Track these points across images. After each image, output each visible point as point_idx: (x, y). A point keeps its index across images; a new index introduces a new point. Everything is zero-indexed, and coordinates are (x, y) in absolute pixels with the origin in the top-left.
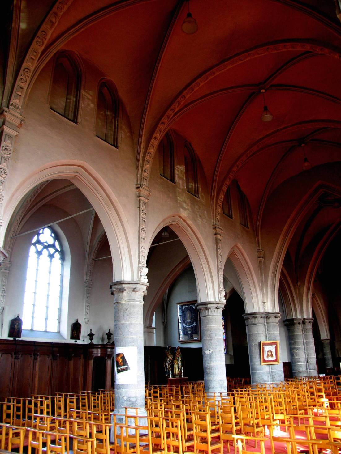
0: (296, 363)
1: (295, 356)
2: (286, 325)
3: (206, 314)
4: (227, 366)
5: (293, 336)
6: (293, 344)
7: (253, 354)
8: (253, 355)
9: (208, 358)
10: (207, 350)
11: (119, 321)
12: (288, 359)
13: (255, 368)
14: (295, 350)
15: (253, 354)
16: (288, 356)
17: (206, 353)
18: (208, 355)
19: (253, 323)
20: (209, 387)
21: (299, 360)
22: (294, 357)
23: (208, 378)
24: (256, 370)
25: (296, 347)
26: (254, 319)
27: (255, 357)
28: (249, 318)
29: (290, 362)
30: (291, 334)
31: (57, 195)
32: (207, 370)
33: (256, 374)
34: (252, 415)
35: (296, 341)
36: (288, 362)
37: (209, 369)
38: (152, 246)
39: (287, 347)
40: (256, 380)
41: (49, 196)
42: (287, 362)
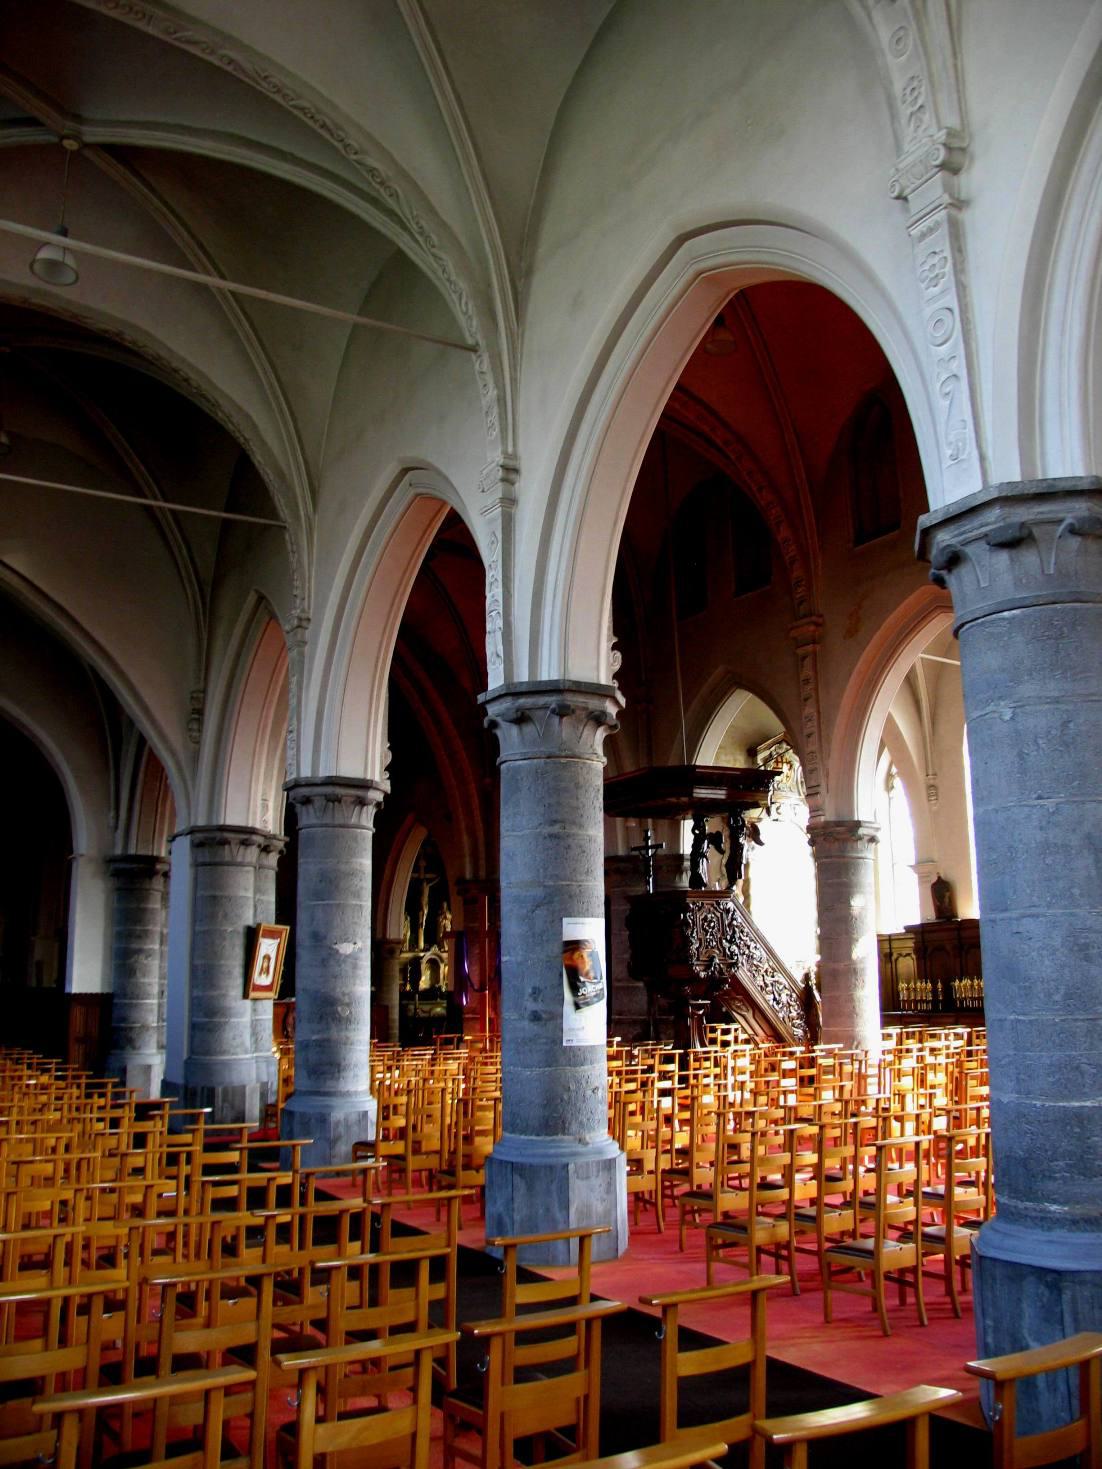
0: (138, 998)
1: (138, 974)
2: (116, 874)
3: (354, 820)
4: (372, 992)
5: (145, 910)
6: (139, 937)
7: (222, 962)
8: (221, 966)
9: (347, 967)
10: (346, 940)
11: (581, 826)
12: (103, 985)
13: (230, 1008)
14: (142, 957)
15: (222, 962)
16: (104, 974)
17: (341, 951)
18: (347, 956)
19: (239, 859)
20: (343, 1064)
21: (148, 988)
22: (133, 980)
23: (343, 1034)
24: (224, 1015)
25: (146, 947)
26: (242, 848)
27: (230, 973)
28: (229, 843)
29: (108, 994)
30: (133, 906)
31: (364, 216)
32: (339, 1009)
33: (227, 1027)
34: (189, 1167)
35: (150, 927)
36: (102, 994)
37: (348, 1005)
38: (159, 496)
39: (105, 943)
40: (225, 1047)
41: (363, 198)
42: (97, 994)
